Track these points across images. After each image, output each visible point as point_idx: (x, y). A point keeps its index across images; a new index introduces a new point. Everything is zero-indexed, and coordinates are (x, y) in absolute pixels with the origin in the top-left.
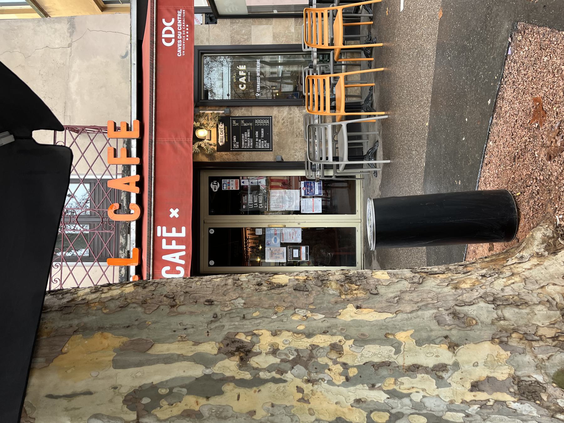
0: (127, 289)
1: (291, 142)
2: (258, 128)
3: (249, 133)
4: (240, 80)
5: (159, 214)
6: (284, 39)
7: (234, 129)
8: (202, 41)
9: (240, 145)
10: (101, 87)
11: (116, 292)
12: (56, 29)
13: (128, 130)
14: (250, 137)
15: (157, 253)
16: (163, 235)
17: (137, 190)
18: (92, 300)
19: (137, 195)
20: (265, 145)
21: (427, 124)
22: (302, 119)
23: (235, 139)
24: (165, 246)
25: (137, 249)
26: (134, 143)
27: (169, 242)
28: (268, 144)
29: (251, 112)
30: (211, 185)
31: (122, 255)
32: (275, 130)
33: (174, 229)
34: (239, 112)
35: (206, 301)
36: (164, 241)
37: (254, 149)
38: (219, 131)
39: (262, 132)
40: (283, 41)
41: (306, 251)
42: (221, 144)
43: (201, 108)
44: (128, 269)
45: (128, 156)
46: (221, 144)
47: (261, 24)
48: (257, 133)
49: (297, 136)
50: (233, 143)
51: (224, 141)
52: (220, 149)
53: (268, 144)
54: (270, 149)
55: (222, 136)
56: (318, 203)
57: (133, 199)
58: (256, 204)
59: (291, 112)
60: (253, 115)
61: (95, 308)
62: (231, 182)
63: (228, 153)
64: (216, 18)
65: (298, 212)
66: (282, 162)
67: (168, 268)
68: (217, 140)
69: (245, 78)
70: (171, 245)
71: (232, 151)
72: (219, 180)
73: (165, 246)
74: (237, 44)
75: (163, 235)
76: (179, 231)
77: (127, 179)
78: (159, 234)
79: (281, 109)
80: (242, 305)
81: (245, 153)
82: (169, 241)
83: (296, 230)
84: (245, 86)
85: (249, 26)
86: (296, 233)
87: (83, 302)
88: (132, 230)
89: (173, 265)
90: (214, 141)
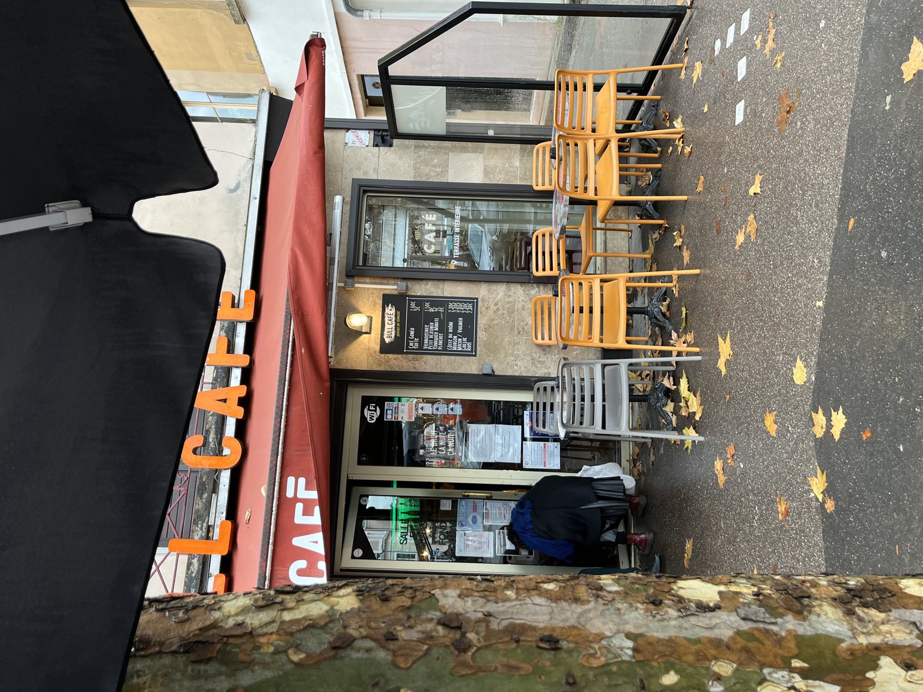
0: (342, 601)
1: (509, 343)
2: (454, 317)
3: (437, 325)
7: (412, 317)
8: (365, 173)
9: (421, 343)
11: (316, 609)
13: (233, 306)
14: (439, 332)
17: (240, 412)
18: (261, 627)
19: (238, 421)
20: (464, 346)
21: (820, 304)
22: (530, 306)
23: (412, 333)
25: (229, 523)
26: (241, 330)
28: (469, 344)
29: (443, 290)
30: (366, 410)
31: (198, 534)
32: (482, 321)
34: (422, 289)
35: (542, 640)
36: (299, 507)
37: (445, 351)
38: (386, 319)
39: (461, 323)
40: (499, 179)
42: (387, 340)
43: (356, 279)
44: (205, 562)
45: (228, 352)
46: (387, 340)
47: (465, 150)
48: (451, 324)
49: (519, 332)
50: (408, 339)
51: (393, 335)
53: (469, 344)
54: (473, 353)
55: (390, 327)
57: (230, 429)
58: (443, 449)
59: (511, 293)
60: (445, 295)
61: (272, 649)
63: (400, 356)
64: (392, 138)
66: (492, 375)
67: (302, 564)
68: (382, 334)
71: (407, 353)
72: (380, 402)
74: (424, 179)
75: (299, 496)
77: (222, 392)
78: (290, 494)
79: (494, 287)
80: (630, 652)
81: (430, 357)
84: (433, 246)
85: (445, 153)
87: (239, 631)
88: (221, 486)
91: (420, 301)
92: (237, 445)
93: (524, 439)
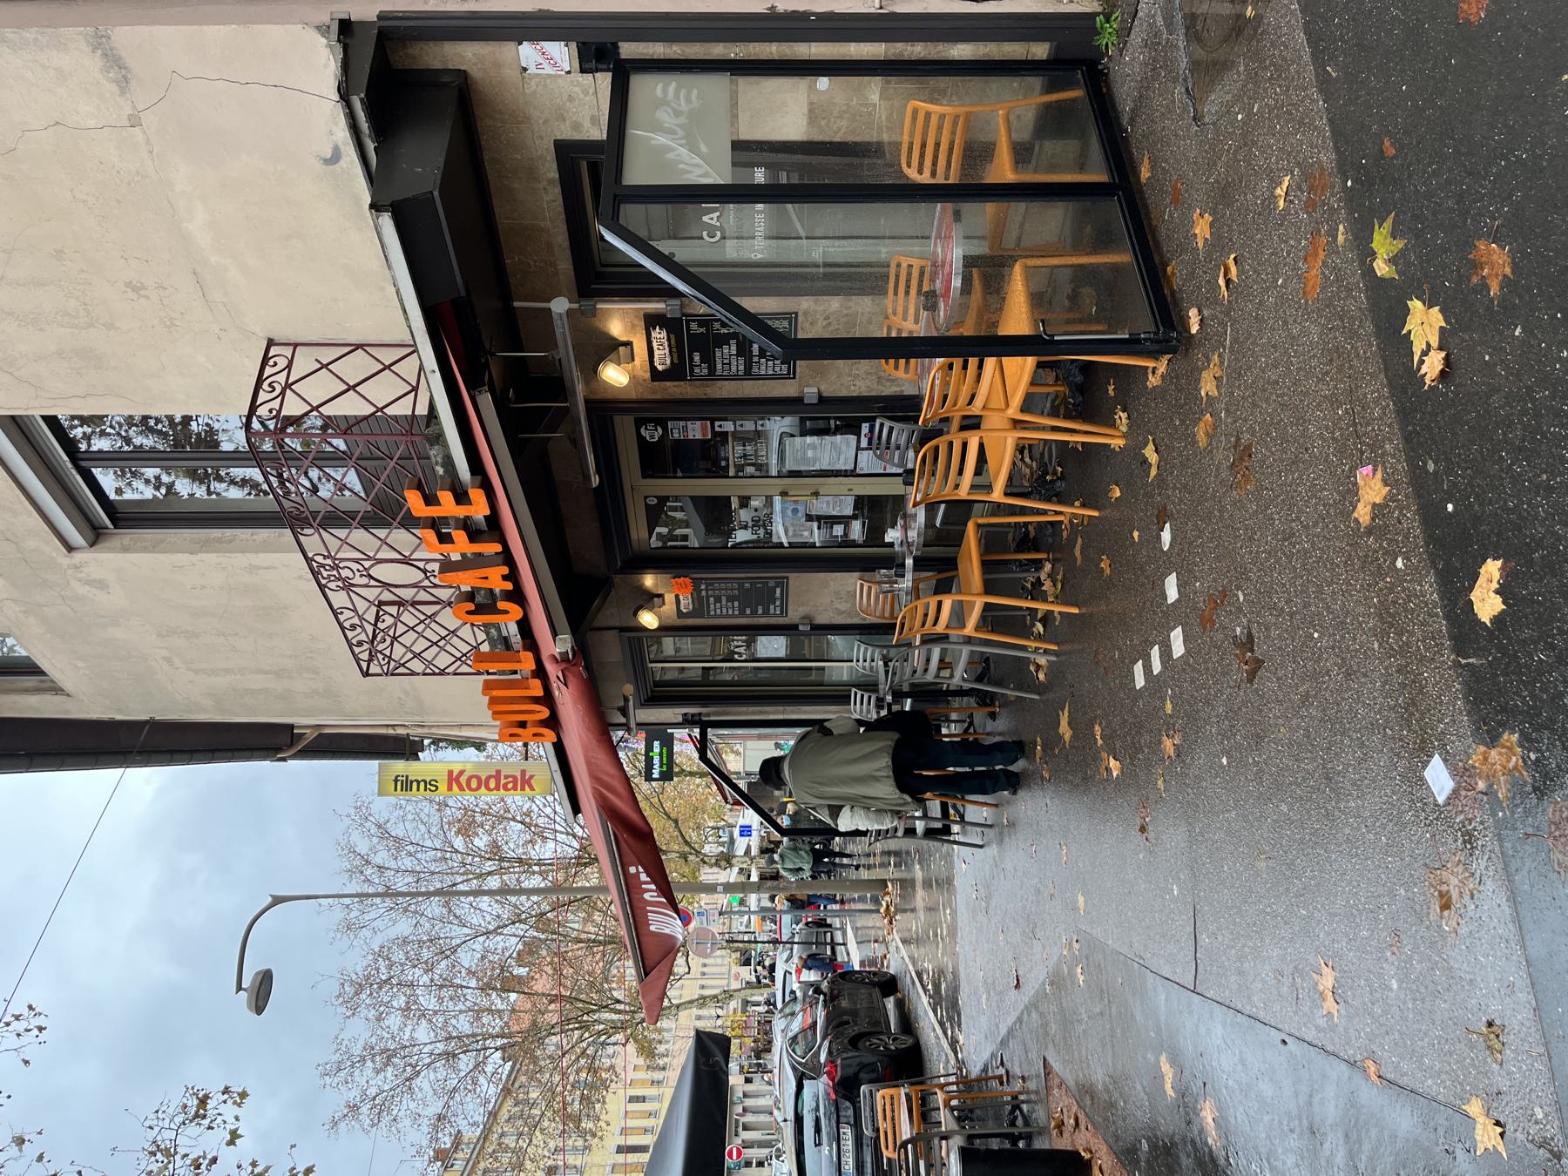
6: (844, 123)
19: (518, 623)
23: (697, 358)
37: (748, 374)
38: (655, 345)
42: (660, 368)
93: (858, 448)
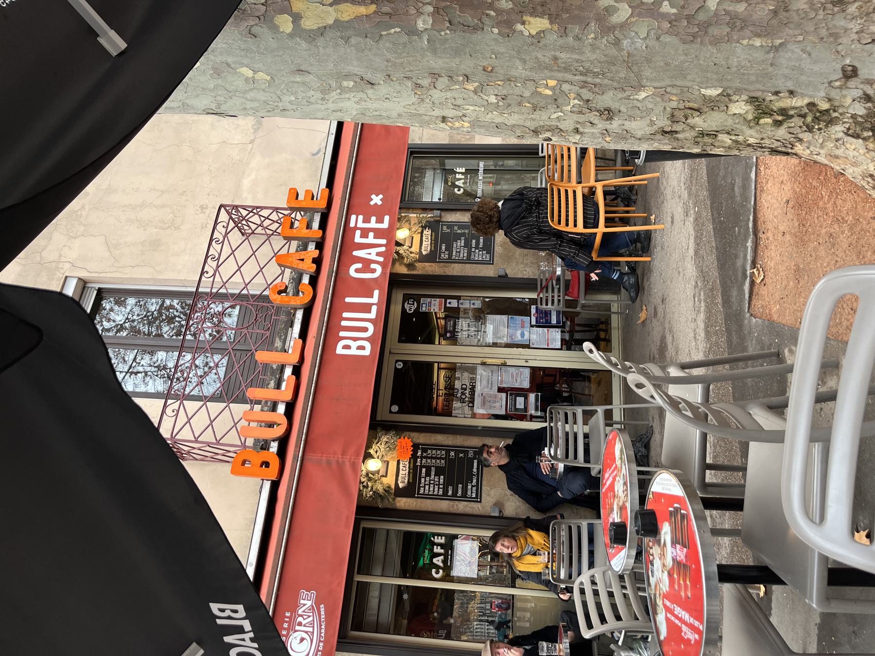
4: (435, 560)
5: (356, 201)
9: (450, 255)
10: (281, 185)
12: (238, 125)
15: (346, 245)
16: (358, 226)
23: (443, 248)
24: (358, 239)
27: (365, 233)
28: (488, 256)
33: (373, 219)
36: (358, 233)
37: (469, 261)
38: (424, 238)
39: (481, 241)
41: (537, 400)
42: (424, 253)
46: (424, 253)
48: (474, 241)
51: (406, 481)
52: (423, 259)
53: (488, 256)
54: (491, 262)
55: (404, 472)
56: (556, 336)
62: (433, 302)
65: (527, 346)
67: (359, 266)
68: (397, 479)
69: (463, 181)
70: (367, 237)
72: (417, 298)
73: (358, 239)
75: (358, 226)
76: (380, 221)
77: (302, 254)
78: (352, 224)
82: (365, 233)
83: (521, 369)
86: (521, 374)
89: (367, 265)
90: (415, 248)
91: (451, 225)
92: (310, 289)
